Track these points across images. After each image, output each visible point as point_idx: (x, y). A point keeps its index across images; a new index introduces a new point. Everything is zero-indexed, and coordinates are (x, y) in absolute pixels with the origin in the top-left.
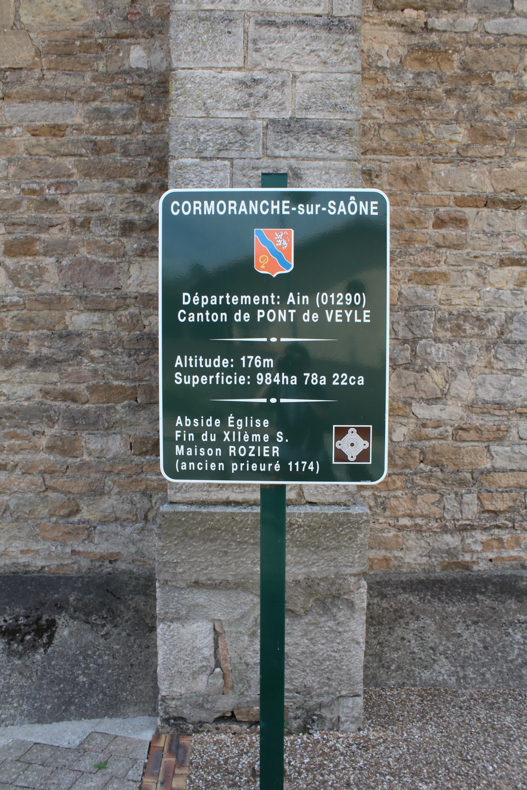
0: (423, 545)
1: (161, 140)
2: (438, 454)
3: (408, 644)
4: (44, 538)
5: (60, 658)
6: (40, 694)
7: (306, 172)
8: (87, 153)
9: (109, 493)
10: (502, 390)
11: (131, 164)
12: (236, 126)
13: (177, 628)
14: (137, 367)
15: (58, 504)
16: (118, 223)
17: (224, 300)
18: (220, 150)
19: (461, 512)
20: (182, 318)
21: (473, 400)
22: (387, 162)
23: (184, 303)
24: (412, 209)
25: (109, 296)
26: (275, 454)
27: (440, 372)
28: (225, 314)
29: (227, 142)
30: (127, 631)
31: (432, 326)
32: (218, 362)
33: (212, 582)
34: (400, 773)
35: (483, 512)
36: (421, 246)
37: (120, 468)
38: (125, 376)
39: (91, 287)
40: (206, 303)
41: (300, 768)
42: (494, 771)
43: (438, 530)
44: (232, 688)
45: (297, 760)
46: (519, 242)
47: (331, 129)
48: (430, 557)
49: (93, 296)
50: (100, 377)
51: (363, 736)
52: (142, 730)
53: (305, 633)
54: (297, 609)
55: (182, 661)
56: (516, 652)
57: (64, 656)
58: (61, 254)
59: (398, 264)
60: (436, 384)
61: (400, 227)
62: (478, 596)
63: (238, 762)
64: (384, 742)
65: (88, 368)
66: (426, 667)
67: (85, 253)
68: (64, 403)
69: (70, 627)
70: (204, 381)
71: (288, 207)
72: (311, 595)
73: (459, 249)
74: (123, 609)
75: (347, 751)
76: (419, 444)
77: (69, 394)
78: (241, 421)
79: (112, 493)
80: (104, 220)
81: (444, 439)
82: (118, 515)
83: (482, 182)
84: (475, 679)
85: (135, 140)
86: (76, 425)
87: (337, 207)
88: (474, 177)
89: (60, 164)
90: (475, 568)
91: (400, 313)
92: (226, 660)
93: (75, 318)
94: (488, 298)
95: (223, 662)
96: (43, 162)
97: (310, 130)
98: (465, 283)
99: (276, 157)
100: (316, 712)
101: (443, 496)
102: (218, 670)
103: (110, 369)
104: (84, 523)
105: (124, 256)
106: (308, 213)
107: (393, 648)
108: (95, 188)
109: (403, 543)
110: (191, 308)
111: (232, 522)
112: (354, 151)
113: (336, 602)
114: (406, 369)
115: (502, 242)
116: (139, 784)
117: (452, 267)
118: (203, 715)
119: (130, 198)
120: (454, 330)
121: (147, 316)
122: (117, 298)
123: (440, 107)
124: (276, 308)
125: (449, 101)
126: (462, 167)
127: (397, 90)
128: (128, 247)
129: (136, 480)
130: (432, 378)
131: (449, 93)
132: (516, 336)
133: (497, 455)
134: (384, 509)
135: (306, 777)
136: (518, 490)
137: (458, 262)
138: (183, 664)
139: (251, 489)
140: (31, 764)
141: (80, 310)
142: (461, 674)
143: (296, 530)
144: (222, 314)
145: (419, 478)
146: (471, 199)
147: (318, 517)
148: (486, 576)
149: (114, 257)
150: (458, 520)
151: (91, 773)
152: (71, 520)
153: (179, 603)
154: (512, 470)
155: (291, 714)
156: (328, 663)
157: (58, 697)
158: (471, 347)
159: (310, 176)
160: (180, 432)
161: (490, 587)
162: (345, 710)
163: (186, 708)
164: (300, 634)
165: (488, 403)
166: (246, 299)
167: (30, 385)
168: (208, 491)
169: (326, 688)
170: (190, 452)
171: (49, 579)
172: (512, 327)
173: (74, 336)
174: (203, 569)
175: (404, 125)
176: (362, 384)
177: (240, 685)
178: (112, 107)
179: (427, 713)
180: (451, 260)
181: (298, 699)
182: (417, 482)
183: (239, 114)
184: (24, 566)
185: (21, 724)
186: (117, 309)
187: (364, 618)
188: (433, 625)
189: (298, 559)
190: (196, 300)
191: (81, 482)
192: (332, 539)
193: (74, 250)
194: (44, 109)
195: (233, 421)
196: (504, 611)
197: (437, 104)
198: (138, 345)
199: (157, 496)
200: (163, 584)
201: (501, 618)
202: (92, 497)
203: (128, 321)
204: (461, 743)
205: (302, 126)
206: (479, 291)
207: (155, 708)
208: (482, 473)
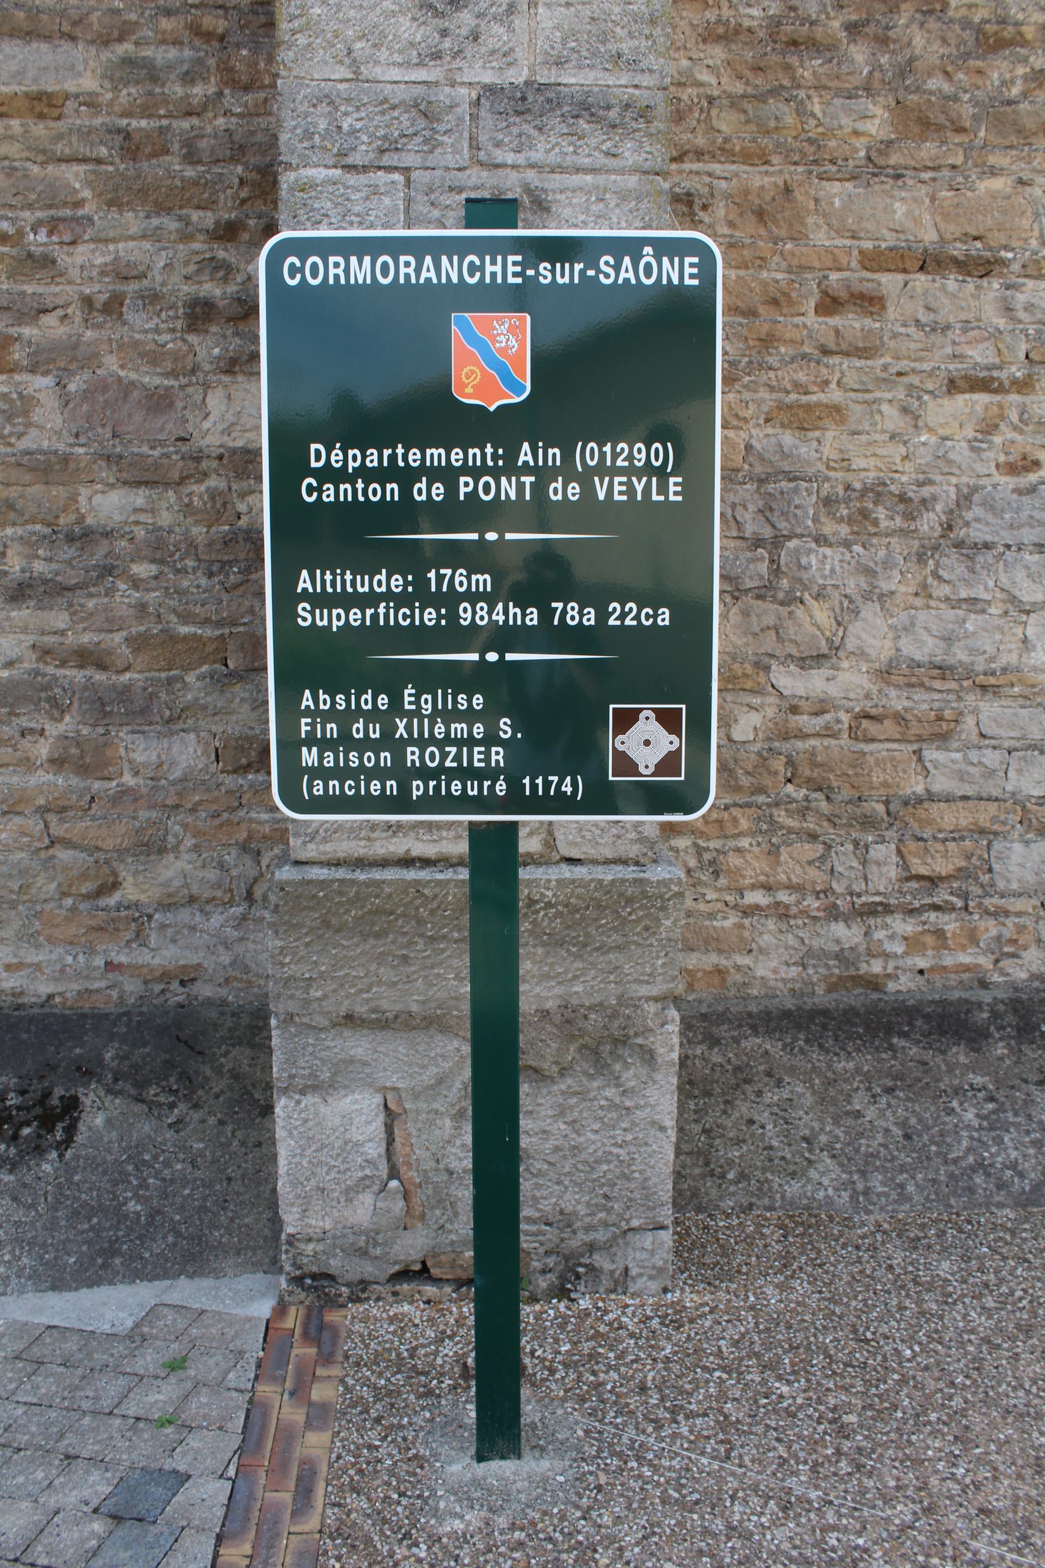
0: (791, 943)
1: (262, 130)
2: (821, 765)
3: (760, 1131)
4: (49, 940)
5: (89, 1169)
6: (53, 1237)
7: (558, 196)
8: (112, 156)
9: (176, 848)
10: (948, 639)
11: (203, 181)
12: (415, 100)
13: (314, 1105)
14: (225, 597)
15: (75, 873)
16: (180, 304)
17: (393, 457)
18: (383, 152)
19: (866, 879)
20: (310, 495)
21: (891, 661)
22: (725, 178)
23: (314, 464)
24: (773, 275)
25: (167, 456)
26: (497, 761)
27: (826, 605)
28: (395, 486)
29: (396, 134)
30: (219, 1115)
31: (811, 512)
32: (382, 581)
33: (379, 1015)
34: (740, 1365)
35: (908, 879)
36: (791, 352)
37: (197, 798)
38: (203, 615)
39: (128, 437)
40: (357, 464)
41: (552, 1361)
42: (914, 1357)
43: (821, 914)
44: (422, 1217)
45: (548, 1348)
46: (986, 344)
47: (608, 108)
48: (804, 967)
49: (133, 454)
50: (153, 619)
51: (673, 1302)
52: (252, 1298)
53: (562, 1112)
54: (545, 1065)
55: (325, 1169)
56: (964, 1143)
57: (98, 1165)
58: (65, 369)
59: (745, 387)
60: (819, 628)
61: (751, 313)
62: (895, 1040)
63: (436, 1353)
64: (711, 1312)
65: (127, 601)
66: (793, 1175)
67: (115, 367)
68: (82, 672)
69: (106, 1109)
70: (355, 620)
71: (518, 269)
72: (572, 1038)
73: (866, 358)
74: (209, 1073)
75: (641, 1330)
76: (785, 747)
77: (91, 653)
78: (429, 697)
79: (182, 848)
80: (152, 299)
81: (834, 736)
82: (195, 890)
83: (915, 221)
84: (886, 1195)
85: (209, 130)
86: (106, 714)
87: (617, 268)
88: (900, 209)
89: (56, 179)
90: (891, 986)
91: (748, 486)
92: (409, 1164)
93: (98, 499)
94: (924, 457)
95: (403, 1169)
96: (19, 174)
97: (566, 109)
98: (879, 427)
99: (498, 166)
100: (582, 1260)
101: (830, 847)
102: (394, 1184)
103: (171, 603)
104: (128, 908)
105: (193, 372)
106: (560, 281)
107: (731, 1139)
108: (131, 232)
109: (753, 940)
110: (328, 474)
111: (416, 898)
112: (656, 154)
113: (620, 1052)
114: (759, 597)
115: (954, 343)
116: (248, 1396)
117: (852, 394)
118: (368, 1269)
119: (203, 253)
120: (855, 521)
121: (243, 495)
122: (183, 458)
123: (835, 61)
124: (496, 473)
125: (852, 48)
126: (877, 187)
127: (746, 23)
128: (202, 354)
129: (229, 823)
130: (811, 617)
131: (853, 29)
132: (977, 533)
133: (936, 768)
134: (716, 874)
135: (563, 1378)
136: (975, 836)
137: (863, 383)
138: (328, 1173)
139: (452, 833)
140: (43, 1363)
141: (108, 484)
142: (860, 1187)
143: (542, 913)
144: (389, 487)
145: (783, 813)
146: (893, 255)
147: (584, 887)
148: (911, 1002)
149: (173, 374)
150: (859, 895)
151: (156, 1377)
152: (102, 902)
153: (316, 1058)
154: (965, 798)
155: (535, 1264)
156: (605, 1167)
157: (89, 1242)
158: (889, 554)
159: (565, 206)
160: (309, 720)
161: (919, 1023)
162: (638, 1254)
163: (335, 1255)
164: (550, 1112)
165: (919, 666)
166: (435, 454)
167: (11, 636)
168: (369, 839)
169: (602, 1215)
170: (329, 761)
171: (64, 1020)
172: (969, 516)
173: (98, 537)
174: (361, 991)
175: (760, 98)
176: (667, 623)
177: (438, 1212)
178: (159, 57)
179: (794, 1258)
180: (850, 381)
181: (549, 1236)
182: (781, 820)
183: (421, 75)
184: (13, 995)
185: (21, 1292)
186: (182, 481)
187: (675, 1081)
188: (808, 1095)
189: (546, 968)
190: (336, 457)
191: (121, 828)
192: (611, 929)
193: (91, 360)
194: (14, 57)
195: (413, 699)
196: (943, 1067)
197: (828, 55)
198: (227, 554)
199: (271, 854)
200: (284, 1021)
201: (938, 1080)
202: (142, 858)
203: (205, 504)
204: (856, 1310)
205: (549, 101)
206: (905, 443)
207: (275, 1258)
208: (906, 803)
